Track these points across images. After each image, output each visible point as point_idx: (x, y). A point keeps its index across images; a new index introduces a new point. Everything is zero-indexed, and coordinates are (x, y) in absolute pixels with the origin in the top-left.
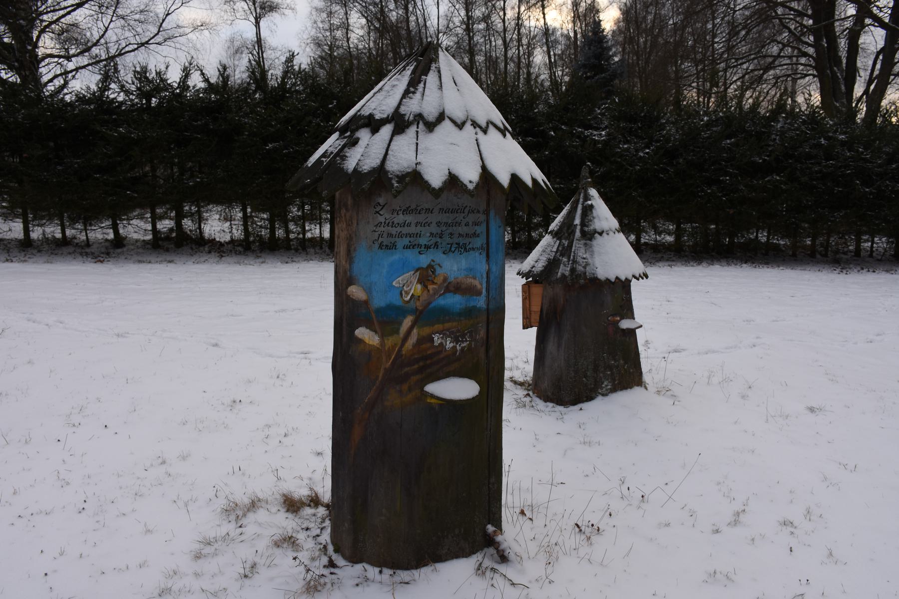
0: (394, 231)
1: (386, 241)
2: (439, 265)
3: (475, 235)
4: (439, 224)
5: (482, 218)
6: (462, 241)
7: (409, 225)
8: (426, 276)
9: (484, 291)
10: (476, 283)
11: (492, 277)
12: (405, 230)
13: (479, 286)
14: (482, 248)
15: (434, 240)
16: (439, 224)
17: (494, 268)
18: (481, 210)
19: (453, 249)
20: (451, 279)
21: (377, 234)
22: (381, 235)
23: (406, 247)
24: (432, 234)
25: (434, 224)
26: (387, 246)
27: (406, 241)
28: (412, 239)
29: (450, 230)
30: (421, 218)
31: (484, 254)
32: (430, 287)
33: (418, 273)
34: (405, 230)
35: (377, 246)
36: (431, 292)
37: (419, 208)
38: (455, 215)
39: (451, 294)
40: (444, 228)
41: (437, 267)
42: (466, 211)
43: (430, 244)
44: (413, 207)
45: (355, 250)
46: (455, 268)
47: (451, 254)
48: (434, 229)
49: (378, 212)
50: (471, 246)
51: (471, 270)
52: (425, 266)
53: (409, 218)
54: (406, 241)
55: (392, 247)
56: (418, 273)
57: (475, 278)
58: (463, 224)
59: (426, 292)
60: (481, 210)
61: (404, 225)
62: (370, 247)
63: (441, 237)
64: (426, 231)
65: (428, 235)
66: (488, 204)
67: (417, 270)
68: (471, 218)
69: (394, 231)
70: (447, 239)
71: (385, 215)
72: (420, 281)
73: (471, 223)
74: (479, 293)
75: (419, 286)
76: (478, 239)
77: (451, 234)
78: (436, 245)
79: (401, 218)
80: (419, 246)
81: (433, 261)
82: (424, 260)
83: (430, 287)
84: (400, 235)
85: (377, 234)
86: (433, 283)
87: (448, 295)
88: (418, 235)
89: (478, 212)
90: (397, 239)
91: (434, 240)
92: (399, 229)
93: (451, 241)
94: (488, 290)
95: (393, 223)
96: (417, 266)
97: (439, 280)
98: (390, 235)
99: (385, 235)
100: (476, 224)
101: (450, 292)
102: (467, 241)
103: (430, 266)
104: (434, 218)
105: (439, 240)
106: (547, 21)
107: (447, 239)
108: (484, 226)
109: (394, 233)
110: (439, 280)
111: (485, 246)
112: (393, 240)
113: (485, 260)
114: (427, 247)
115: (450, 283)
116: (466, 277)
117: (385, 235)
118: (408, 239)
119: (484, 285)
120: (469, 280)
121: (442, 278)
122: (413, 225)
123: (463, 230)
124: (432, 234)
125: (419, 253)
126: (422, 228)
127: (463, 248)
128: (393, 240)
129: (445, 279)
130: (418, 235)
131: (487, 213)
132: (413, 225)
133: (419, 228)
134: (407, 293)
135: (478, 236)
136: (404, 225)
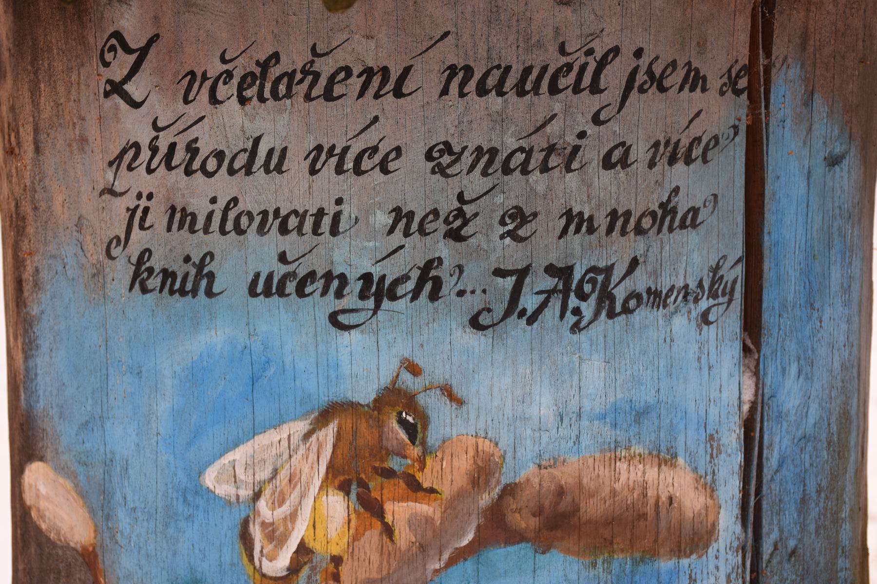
0: (200, 194)
1: (167, 248)
2: (448, 392)
3: (668, 216)
4: (441, 157)
5: (721, 113)
6: (582, 254)
7: (276, 163)
8: (377, 442)
9: (728, 524)
10: (679, 485)
11: (778, 442)
12: (258, 192)
13: (692, 501)
14: (715, 285)
15: (415, 252)
16: (441, 157)
17: (789, 393)
18: (714, 70)
19: (529, 301)
20: (521, 467)
21: (120, 206)
22: (138, 217)
23: (264, 287)
24: (401, 217)
25: (414, 160)
26: (168, 275)
27: (262, 253)
28: (292, 244)
29: (514, 191)
30: (339, 122)
31: (731, 320)
32: (400, 511)
33: (328, 434)
34: (258, 192)
35: (121, 271)
36: (404, 537)
37: (326, 67)
38: (545, 103)
39: (521, 551)
40: (475, 184)
41: (435, 405)
42: (614, 77)
43: (391, 270)
44: (294, 58)
45: (37, 286)
46: (543, 406)
47: (517, 328)
48: (415, 186)
49: (116, 88)
50: (640, 281)
51: (640, 415)
52: (366, 394)
53: (278, 124)
54: (262, 253)
55: (192, 281)
56: (328, 434)
57: (666, 459)
58: (592, 154)
59: (373, 537)
60: (714, 70)
61: (251, 160)
62: (98, 273)
63: (455, 235)
64: (370, 199)
65: (384, 219)
66: (762, 35)
67: (325, 416)
68: (647, 119)
69: (200, 194)
70: (492, 245)
71: (156, 104)
72: (342, 476)
73: (640, 152)
74: (695, 539)
75: (338, 506)
76: (691, 237)
77: (519, 217)
78: (429, 281)
79: (228, 124)
80: (335, 282)
81: (414, 369)
82: (362, 362)
83: (400, 511)
84: (232, 221)
85: (120, 206)
86: (415, 487)
87: (501, 556)
88: (328, 222)
89: (695, 80)
90: (214, 241)
91: (415, 252)
92: (224, 186)
93: (513, 255)
94: (751, 512)
95: (192, 150)
96: (324, 396)
97: (448, 473)
98: (181, 218)
99: (158, 217)
100: (674, 153)
101: (514, 537)
102: (616, 251)
103: (394, 398)
104: (413, 122)
105: (444, 250)
106: (116, 183)
107: (492, 245)
108: (732, 162)
109: (200, 207)
110: (448, 473)
111: (735, 273)
112: (195, 245)
113: (732, 351)
114: (378, 290)
115: (510, 490)
116: (613, 453)
117: (158, 217)
118: (274, 242)
119: (730, 489)
120: (629, 475)
121: (463, 464)
122: (296, 164)
123: (593, 189)
124: (401, 217)
125: (333, 319)
126: (348, 185)
127: (588, 295)
128: (195, 245)
129: (483, 472)
130: (328, 222)
131: (753, 84)
132: (296, 164)
133: (326, 188)
134: (275, 536)
135: (692, 220)
136: (251, 160)
